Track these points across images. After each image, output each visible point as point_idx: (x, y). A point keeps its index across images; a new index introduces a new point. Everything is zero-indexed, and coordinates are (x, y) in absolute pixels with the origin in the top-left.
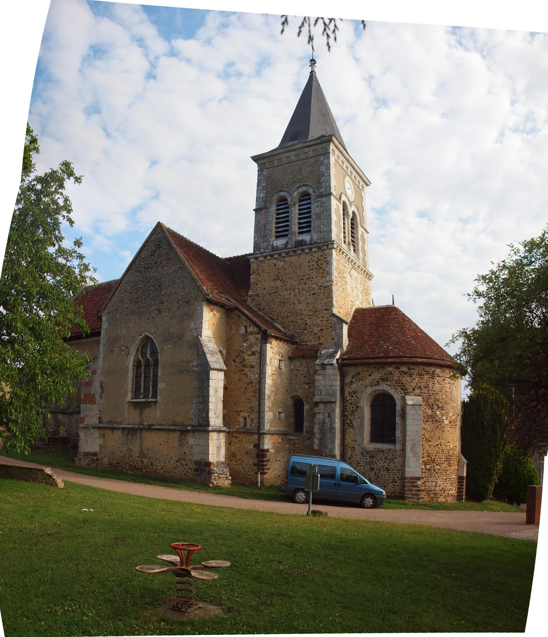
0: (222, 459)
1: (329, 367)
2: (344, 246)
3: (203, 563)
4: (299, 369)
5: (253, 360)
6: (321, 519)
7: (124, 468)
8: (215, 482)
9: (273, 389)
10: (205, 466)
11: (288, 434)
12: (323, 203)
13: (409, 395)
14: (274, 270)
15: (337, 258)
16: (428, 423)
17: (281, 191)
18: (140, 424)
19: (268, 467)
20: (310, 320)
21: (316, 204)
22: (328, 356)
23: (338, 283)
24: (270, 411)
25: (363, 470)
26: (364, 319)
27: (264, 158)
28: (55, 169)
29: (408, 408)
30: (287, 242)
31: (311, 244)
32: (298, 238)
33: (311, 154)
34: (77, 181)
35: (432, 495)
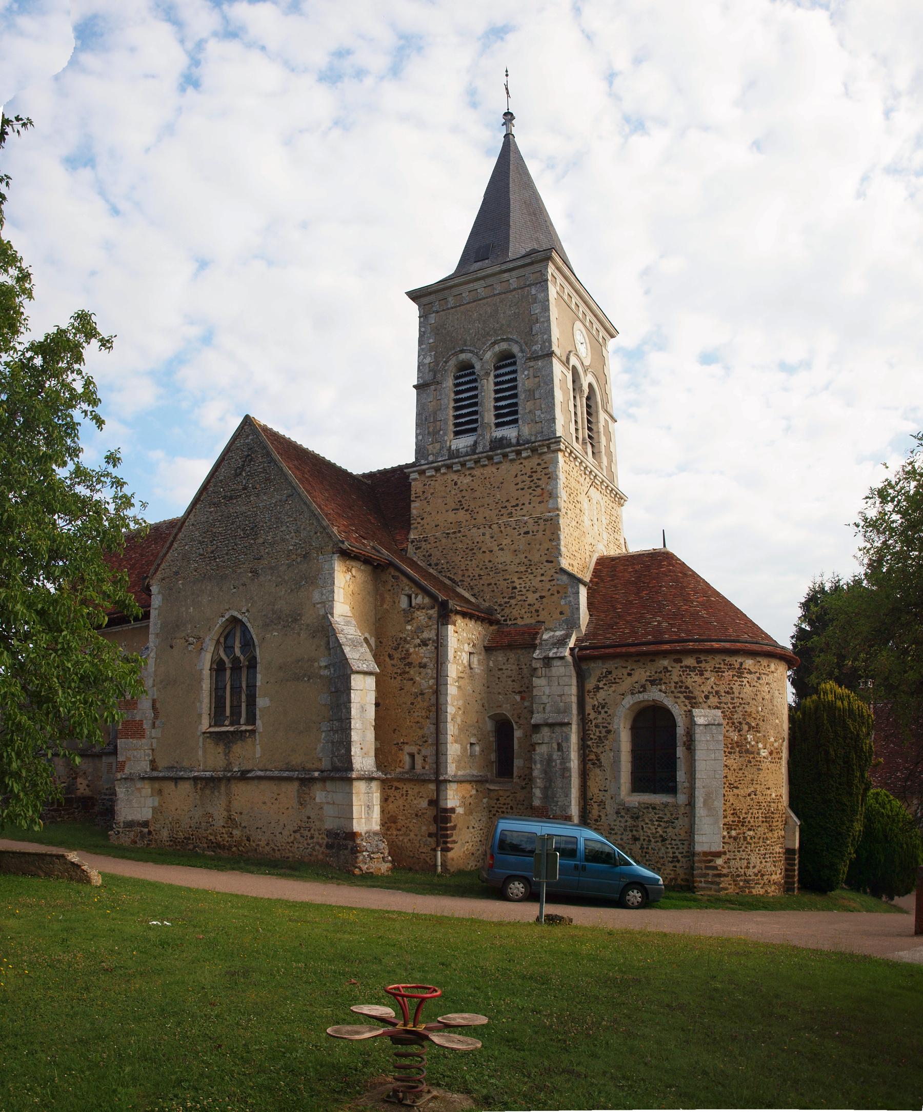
0: (376, 827)
1: (557, 663)
2: (575, 444)
3: (439, 1019)
4: (504, 667)
5: (424, 654)
6: (558, 931)
7: (198, 847)
8: (364, 867)
9: (461, 703)
10: (345, 839)
11: (487, 781)
12: (539, 370)
13: (698, 708)
14: (453, 492)
15: (566, 467)
16: (733, 756)
17: (462, 351)
18: (225, 771)
19: (454, 838)
20: (521, 581)
21: (526, 373)
22: (555, 644)
23: (569, 512)
24: (456, 742)
25: (620, 842)
26: (615, 575)
27: (430, 293)
28: (64, 326)
29: (698, 730)
30: (476, 442)
31: (518, 444)
32: (494, 434)
33: (514, 283)
34: (103, 345)
35: (741, 884)
